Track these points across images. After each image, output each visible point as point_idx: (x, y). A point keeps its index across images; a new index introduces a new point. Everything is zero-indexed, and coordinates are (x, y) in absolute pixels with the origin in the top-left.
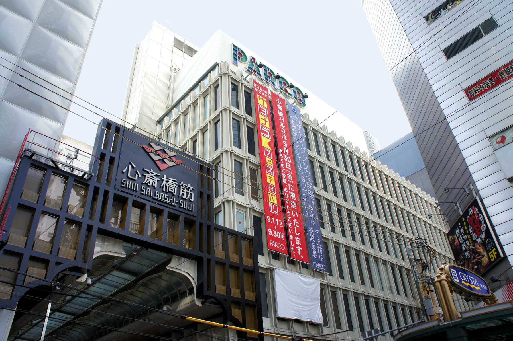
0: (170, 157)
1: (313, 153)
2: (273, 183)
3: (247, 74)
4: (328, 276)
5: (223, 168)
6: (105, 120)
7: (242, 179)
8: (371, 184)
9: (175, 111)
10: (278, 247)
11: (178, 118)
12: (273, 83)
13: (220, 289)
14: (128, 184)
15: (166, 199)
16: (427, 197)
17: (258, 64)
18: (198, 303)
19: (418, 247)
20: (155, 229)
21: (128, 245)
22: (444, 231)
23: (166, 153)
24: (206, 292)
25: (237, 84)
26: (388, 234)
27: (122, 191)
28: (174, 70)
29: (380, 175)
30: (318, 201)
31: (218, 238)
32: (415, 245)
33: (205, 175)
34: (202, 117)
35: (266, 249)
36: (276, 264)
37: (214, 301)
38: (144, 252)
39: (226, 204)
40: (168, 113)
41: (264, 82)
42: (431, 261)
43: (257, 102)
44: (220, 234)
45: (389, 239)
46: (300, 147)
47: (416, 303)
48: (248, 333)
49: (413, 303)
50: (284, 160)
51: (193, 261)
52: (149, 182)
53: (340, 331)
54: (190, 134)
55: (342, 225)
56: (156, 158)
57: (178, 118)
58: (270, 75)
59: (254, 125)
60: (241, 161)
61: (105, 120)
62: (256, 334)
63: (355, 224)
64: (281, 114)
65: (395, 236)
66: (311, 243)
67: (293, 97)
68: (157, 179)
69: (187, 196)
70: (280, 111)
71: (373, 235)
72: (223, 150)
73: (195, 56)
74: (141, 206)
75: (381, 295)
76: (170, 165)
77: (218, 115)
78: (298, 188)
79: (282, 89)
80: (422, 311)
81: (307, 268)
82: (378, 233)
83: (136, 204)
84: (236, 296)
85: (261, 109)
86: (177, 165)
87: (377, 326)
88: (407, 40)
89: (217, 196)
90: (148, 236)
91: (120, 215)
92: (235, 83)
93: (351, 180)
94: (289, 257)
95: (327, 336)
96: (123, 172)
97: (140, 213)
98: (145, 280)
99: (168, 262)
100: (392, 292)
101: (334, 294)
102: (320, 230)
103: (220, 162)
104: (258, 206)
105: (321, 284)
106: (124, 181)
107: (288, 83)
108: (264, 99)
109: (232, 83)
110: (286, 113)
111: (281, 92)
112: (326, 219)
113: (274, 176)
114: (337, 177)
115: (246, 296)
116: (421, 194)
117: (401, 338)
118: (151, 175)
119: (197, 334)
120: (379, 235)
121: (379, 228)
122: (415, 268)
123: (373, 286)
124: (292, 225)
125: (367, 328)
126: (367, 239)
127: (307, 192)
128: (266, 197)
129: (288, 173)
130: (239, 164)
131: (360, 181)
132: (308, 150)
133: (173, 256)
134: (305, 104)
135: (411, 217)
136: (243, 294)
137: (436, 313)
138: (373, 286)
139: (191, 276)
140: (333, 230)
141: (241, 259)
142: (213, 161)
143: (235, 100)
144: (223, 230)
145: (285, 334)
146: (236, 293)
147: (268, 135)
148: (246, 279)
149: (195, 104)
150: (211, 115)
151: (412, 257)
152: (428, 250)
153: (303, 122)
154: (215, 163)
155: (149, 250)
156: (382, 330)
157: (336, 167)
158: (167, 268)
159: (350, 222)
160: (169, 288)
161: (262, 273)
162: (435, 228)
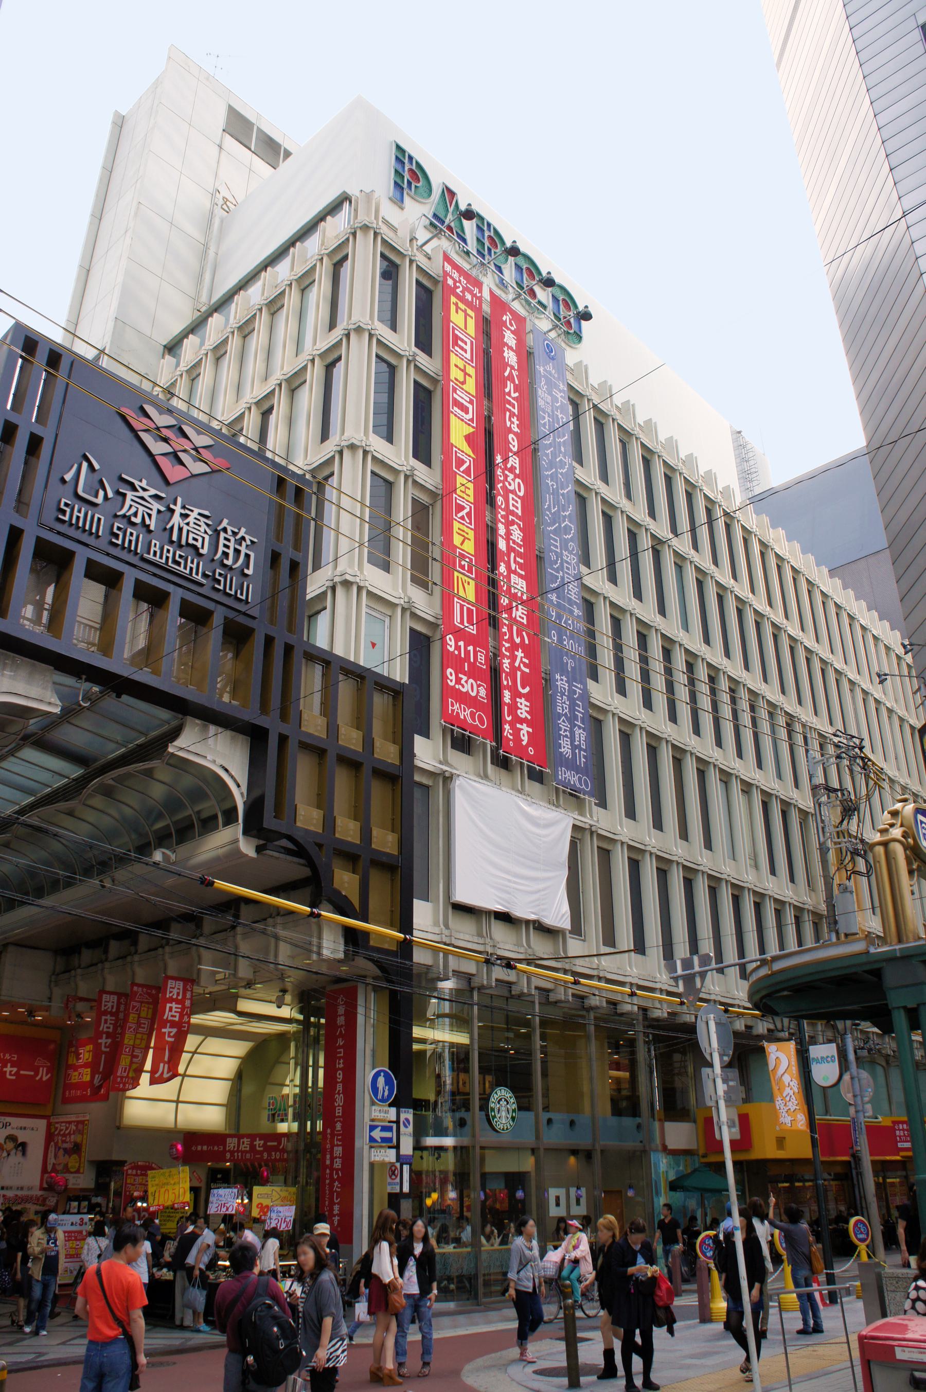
0: (196, 449)
1: (589, 475)
2: (469, 547)
3: (429, 236)
4: (595, 808)
5: (339, 491)
6: (19, 327)
7: (388, 527)
8: (735, 577)
9: (216, 320)
10: (470, 720)
11: (225, 341)
12: (499, 269)
13: (308, 818)
14: (76, 513)
15: (179, 564)
16: (881, 628)
17: (463, 207)
18: (247, 848)
19: (839, 757)
20: (141, 643)
21: (69, 681)
22: (912, 722)
23: (185, 436)
24: (269, 821)
25: (397, 260)
26: (763, 714)
27: (59, 533)
28: (221, 202)
29: (762, 554)
30: (589, 608)
31: (311, 680)
32: (831, 750)
33: (294, 501)
34: (291, 348)
35: (436, 722)
36: (459, 763)
37: (290, 845)
38: (111, 703)
39: (340, 591)
40: (196, 327)
41: (474, 260)
42: (869, 797)
43: (453, 310)
44: (318, 669)
45: (765, 727)
46: (554, 455)
47: (815, 901)
48: (372, 936)
49: (807, 899)
50: (504, 487)
51: (241, 736)
52: (135, 515)
53: (612, 950)
54: (254, 391)
55: (645, 676)
56: (158, 448)
57: (225, 341)
58: (492, 242)
59: (435, 381)
60: (390, 478)
61: (19, 327)
62: (392, 938)
63: (681, 678)
64: (511, 357)
65: (781, 721)
66: (559, 716)
67: (549, 312)
68: (156, 506)
69: (236, 560)
70: (510, 348)
71: (726, 711)
72: (343, 442)
73: (285, 166)
74: (109, 579)
75: (727, 870)
76: (194, 473)
77: (338, 344)
78: (535, 564)
79: (522, 288)
80: (827, 921)
81: (541, 782)
82: (738, 707)
83: (95, 572)
84: (349, 839)
85: (456, 338)
86: (213, 471)
87: (707, 947)
88: (890, 181)
89: (317, 566)
90: (120, 663)
91: (49, 598)
92: (392, 257)
93: (683, 558)
94: (497, 749)
95: (577, 961)
96: (63, 481)
97: (106, 596)
98: (108, 779)
99: (175, 734)
100: (756, 867)
101: (605, 855)
102: (585, 685)
103: (332, 474)
104: (426, 604)
105: (574, 826)
106: (66, 505)
107: (540, 273)
108: (469, 312)
109: (383, 256)
110: (526, 356)
111: (518, 296)
112: (606, 657)
113: (475, 530)
114: (645, 542)
115: (374, 840)
116: (867, 617)
117: (767, 976)
118: (141, 493)
119: (239, 929)
120: (740, 714)
121: (743, 695)
122: (824, 810)
123: (708, 845)
124: (512, 664)
125: (681, 949)
126: (707, 721)
127: (563, 578)
128: (447, 580)
129: (513, 523)
130: (384, 484)
131: (706, 563)
132: (575, 464)
133: (189, 718)
134: (579, 337)
135: (832, 676)
136: (366, 834)
137: (863, 931)
138: (708, 844)
139: (232, 777)
140: (621, 689)
141: (368, 742)
142: (313, 472)
143: (388, 306)
144: (327, 661)
145: (469, 946)
146: (347, 830)
147: (467, 413)
148: (378, 793)
149: (274, 306)
150: (317, 341)
151: (820, 780)
152: (864, 768)
153: (571, 388)
154: (320, 477)
155: (125, 698)
156: (719, 957)
157: (648, 519)
158: (171, 749)
159: (669, 671)
160: (172, 804)
161: (420, 785)
162: (890, 711)
